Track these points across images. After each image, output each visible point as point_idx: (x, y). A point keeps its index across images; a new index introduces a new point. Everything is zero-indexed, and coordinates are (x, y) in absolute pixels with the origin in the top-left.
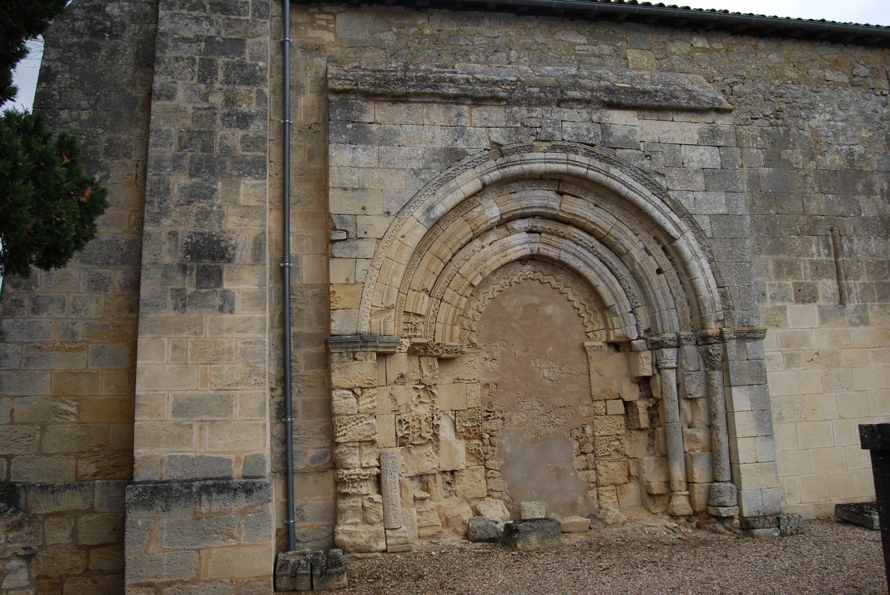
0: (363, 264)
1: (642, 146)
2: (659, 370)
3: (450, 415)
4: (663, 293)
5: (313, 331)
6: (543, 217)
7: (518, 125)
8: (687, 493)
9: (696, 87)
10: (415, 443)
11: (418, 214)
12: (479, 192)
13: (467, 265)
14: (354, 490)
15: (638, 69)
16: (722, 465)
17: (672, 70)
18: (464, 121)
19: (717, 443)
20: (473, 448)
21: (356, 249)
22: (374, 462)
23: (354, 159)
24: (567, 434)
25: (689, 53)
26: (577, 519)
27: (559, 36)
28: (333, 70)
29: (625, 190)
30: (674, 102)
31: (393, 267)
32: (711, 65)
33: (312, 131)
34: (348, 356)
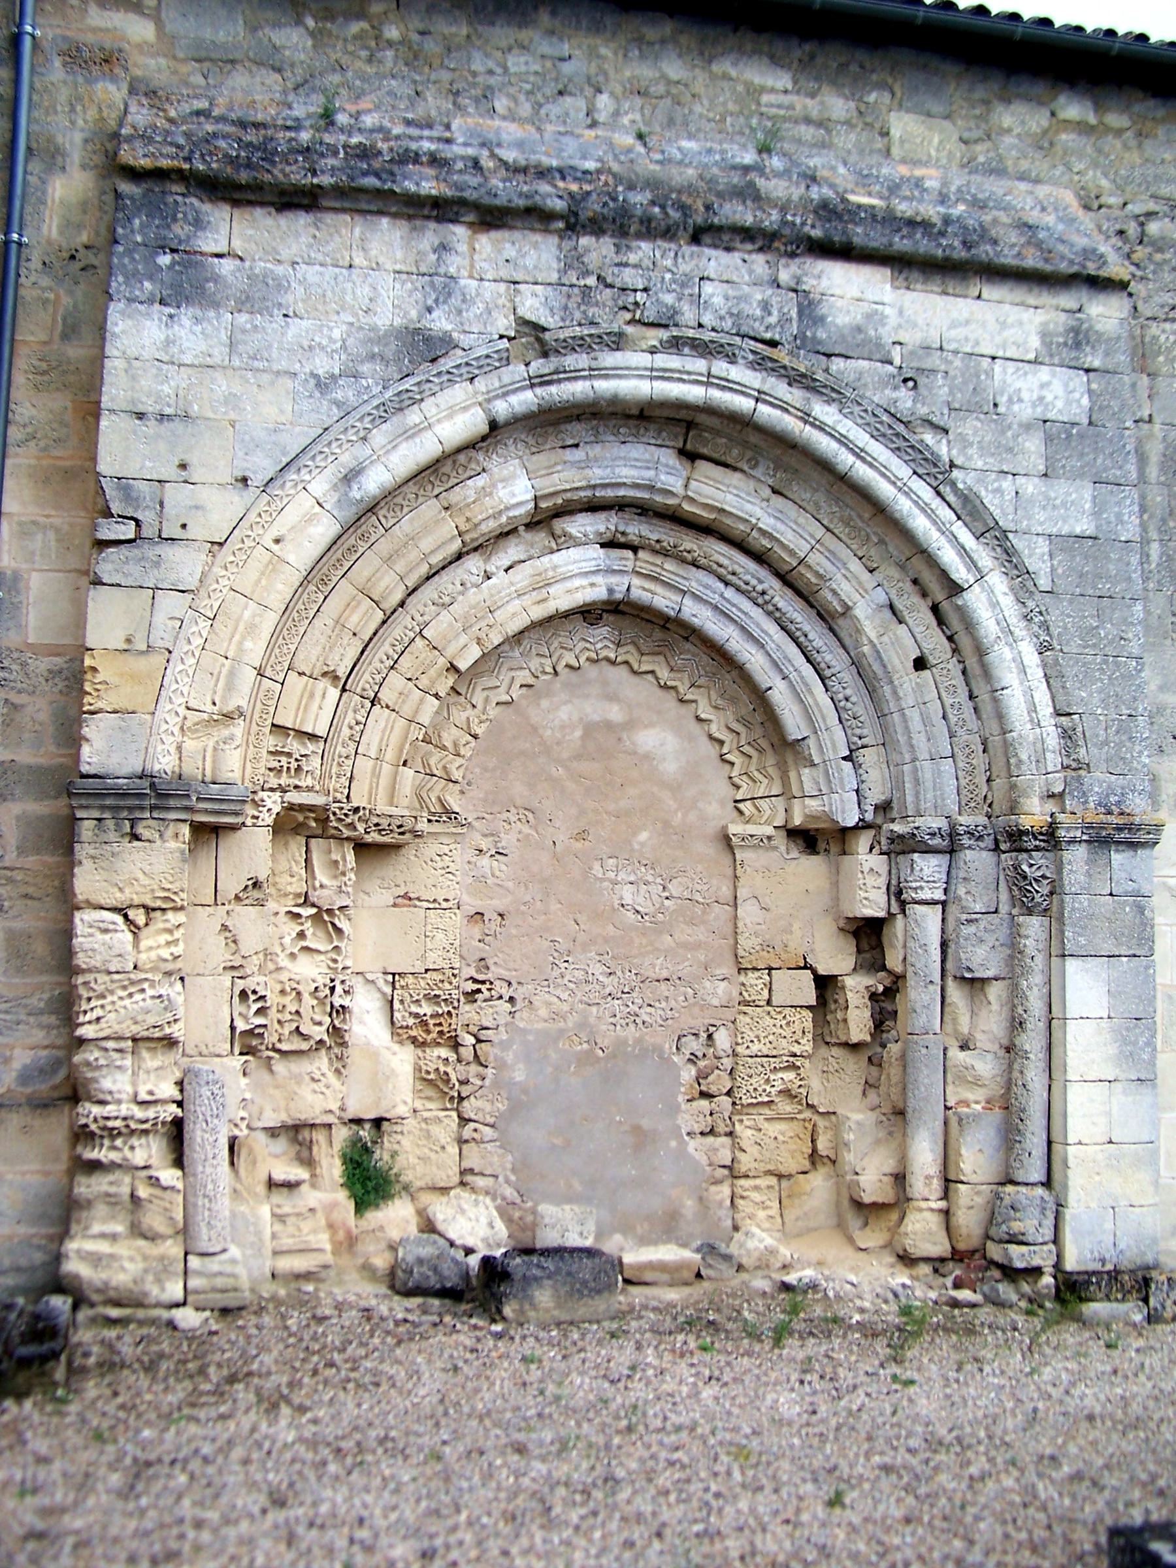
0: (170, 604)
1: (896, 355)
2: (903, 904)
3: (381, 983)
4: (926, 721)
5: (42, 761)
6: (643, 510)
7: (591, 281)
8: (942, 1204)
9: (1050, 219)
10: (284, 1047)
11: (320, 485)
12: (484, 438)
13: (445, 617)
14: (114, 1156)
15: (916, 163)
16: (1028, 1145)
17: (997, 170)
18: (454, 264)
19: (1020, 1091)
20: (432, 1067)
21: (157, 565)
22: (168, 1090)
23: (168, 342)
24: (669, 1046)
25: (1045, 132)
26: (668, 1253)
27: (723, 66)
28: (140, 116)
29: (845, 460)
30: (985, 252)
31: (247, 614)
32: (1095, 165)
33: (78, 265)
34: (118, 828)
